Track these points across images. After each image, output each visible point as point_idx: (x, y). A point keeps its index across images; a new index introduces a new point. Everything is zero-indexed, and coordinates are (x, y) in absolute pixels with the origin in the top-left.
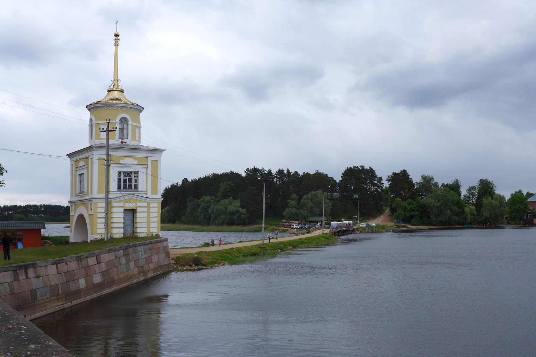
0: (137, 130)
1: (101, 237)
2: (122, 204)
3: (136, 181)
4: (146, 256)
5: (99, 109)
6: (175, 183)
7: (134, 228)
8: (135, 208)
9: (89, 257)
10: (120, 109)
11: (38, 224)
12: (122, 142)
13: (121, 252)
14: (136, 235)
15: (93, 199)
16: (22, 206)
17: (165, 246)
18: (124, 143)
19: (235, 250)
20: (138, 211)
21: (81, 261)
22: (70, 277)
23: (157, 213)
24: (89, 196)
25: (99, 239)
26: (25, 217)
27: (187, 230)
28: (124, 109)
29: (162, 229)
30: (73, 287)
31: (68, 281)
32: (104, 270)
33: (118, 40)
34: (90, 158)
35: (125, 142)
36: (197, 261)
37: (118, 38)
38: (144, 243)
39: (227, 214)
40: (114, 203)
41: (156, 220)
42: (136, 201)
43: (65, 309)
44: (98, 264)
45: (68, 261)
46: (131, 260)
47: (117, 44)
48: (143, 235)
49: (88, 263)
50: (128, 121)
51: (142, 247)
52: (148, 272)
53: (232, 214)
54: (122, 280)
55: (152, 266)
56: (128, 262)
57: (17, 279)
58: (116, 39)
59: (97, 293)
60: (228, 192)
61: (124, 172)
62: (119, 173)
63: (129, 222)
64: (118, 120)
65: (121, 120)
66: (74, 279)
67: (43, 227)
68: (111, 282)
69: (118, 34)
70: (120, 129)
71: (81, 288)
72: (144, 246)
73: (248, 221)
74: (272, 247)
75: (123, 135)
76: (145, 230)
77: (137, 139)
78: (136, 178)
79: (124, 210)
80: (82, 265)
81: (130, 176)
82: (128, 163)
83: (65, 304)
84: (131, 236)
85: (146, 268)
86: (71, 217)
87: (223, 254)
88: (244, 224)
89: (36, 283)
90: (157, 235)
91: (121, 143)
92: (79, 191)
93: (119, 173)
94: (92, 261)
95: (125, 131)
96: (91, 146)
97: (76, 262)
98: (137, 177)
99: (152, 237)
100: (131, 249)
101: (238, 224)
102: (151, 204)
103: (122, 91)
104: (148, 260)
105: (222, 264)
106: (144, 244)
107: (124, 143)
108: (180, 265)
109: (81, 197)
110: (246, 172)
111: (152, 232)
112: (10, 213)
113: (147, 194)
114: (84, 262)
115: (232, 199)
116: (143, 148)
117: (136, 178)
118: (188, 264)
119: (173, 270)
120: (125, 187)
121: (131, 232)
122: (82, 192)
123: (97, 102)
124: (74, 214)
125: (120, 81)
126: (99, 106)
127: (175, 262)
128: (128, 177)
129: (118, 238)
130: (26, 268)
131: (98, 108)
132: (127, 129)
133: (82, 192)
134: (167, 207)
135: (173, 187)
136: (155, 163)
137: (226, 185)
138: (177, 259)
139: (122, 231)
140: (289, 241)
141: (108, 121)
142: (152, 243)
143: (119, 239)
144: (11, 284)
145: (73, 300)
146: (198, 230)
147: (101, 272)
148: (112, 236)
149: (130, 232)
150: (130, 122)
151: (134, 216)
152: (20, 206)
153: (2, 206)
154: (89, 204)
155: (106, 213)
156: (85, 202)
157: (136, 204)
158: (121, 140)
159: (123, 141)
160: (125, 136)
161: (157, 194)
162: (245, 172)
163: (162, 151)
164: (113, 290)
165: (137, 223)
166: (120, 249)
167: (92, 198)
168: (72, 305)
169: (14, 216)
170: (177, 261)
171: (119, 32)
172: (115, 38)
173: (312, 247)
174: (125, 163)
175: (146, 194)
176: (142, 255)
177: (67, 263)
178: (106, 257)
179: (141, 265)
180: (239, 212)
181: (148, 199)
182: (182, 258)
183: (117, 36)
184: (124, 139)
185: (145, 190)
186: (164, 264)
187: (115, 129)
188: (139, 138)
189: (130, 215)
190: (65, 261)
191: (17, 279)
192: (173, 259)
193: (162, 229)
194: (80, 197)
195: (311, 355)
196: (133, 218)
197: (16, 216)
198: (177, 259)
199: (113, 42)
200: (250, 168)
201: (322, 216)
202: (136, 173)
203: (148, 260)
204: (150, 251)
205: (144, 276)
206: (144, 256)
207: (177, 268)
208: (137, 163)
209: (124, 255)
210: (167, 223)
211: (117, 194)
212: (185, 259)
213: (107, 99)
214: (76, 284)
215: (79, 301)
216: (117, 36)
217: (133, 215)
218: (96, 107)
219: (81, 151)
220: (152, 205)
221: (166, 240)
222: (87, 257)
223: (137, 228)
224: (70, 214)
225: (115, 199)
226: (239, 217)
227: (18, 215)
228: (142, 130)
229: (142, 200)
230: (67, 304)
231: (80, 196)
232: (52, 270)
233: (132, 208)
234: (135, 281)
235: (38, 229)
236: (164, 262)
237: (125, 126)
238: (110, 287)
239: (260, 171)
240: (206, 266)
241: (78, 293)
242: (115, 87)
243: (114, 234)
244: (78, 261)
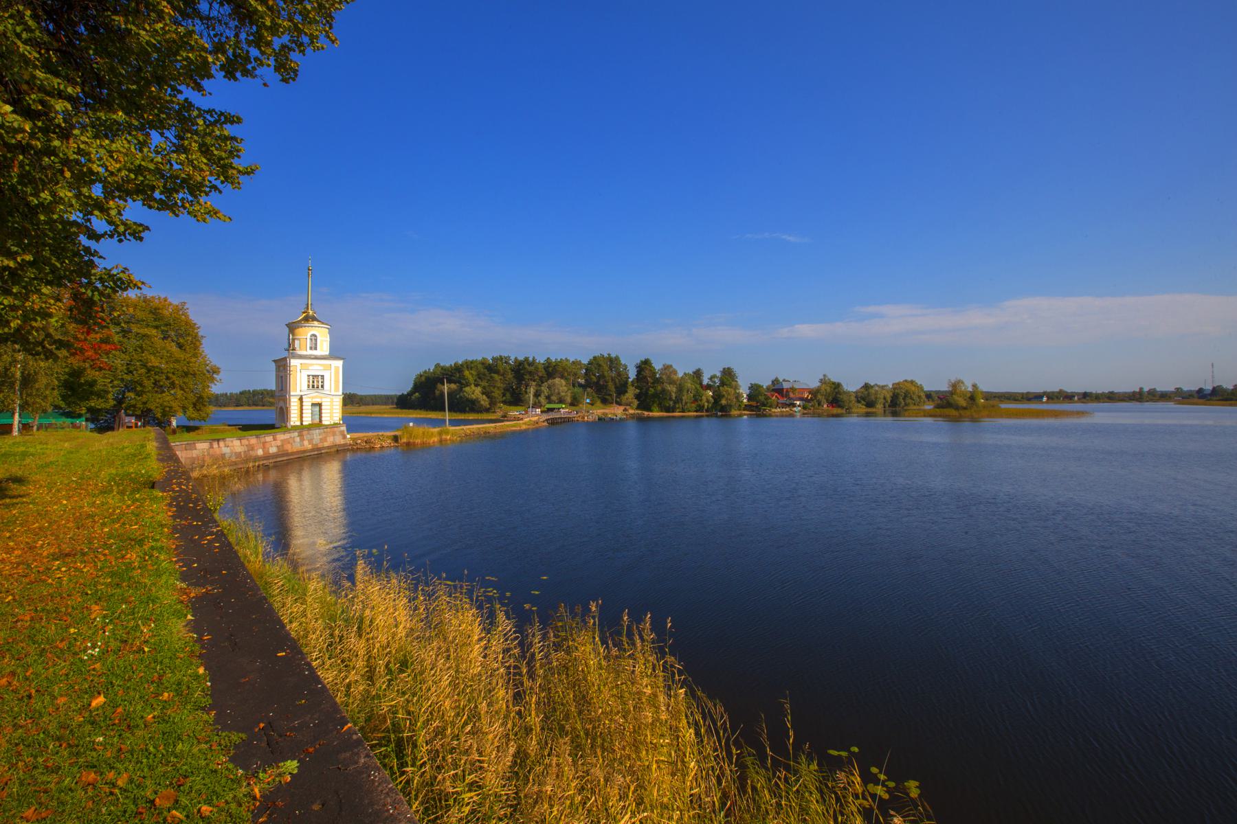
13: (296, 434)
22: (252, 448)
57: (211, 447)
64: (309, 337)
89: (226, 450)
114: (263, 440)
120: (313, 386)
130: (218, 440)
139: (310, 419)
140: (1126, 393)
144: (208, 450)
173: (1102, 416)
191: (211, 447)
201: (445, 411)
202: (323, 376)
232: (237, 443)
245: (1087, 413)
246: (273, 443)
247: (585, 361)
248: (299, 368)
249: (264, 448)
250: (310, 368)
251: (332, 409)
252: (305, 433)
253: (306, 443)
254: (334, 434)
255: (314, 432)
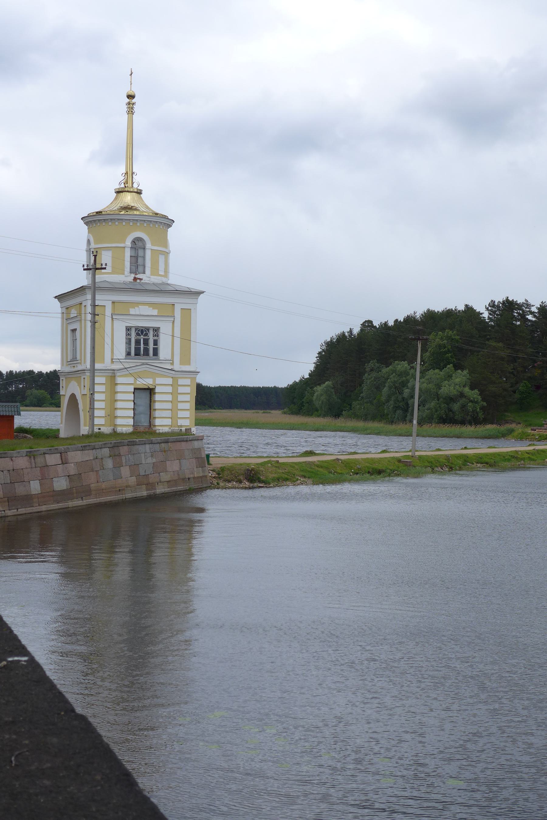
0: (162, 259)
1: (99, 431)
2: (131, 380)
3: (156, 343)
4: (154, 460)
5: (105, 223)
6: (346, 330)
7: (151, 418)
8: (151, 387)
9: (48, 454)
10: (131, 224)
11: (10, 408)
12: (135, 279)
13: (106, 451)
14: (154, 429)
15: (86, 371)
16: (44, 372)
17: (196, 447)
18: (138, 281)
19: (341, 462)
20: (157, 390)
21: (34, 458)
23: (189, 396)
26: (49, 396)
27: (354, 430)
28: (138, 224)
29: (199, 423)
30: (20, 490)
31: (13, 482)
32: (72, 472)
33: (133, 104)
34: (83, 304)
35: (141, 279)
36: (252, 475)
37: (134, 101)
38: (152, 440)
39: (441, 400)
40: (118, 378)
41: (187, 406)
42: (153, 376)
43: (8, 516)
44: (63, 463)
45: (15, 456)
46: (124, 464)
47: (131, 110)
48: (166, 429)
49: (46, 461)
50: (146, 243)
51: (147, 446)
52: (157, 485)
53: (450, 400)
54: (104, 491)
55: (165, 477)
56: (118, 466)
58: (129, 103)
59: (58, 503)
60: (446, 353)
61: (137, 329)
62: (128, 329)
63: (143, 408)
64: (128, 243)
65: (133, 242)
66: (22, 480)
67: (16, 413)
68: (87, 492)
69: (133, 94)
70: (132, 258)
71: (33, 493)
72: (150, 445)
73: (483, 416)
74: (429, 462)
75: (137, 267)
76: (168, 422)
77: (162, 273)
78: (156, 338)
79: (135, 389)
80: (35, 464)
81: (146, 335)
82: (142, 313)
83: (8, 511)
84: (147, 430)
85: (153, 479)
86: (62, 398)
87: (310, 468)
88: (475, 421)
90: (188, 431)
91: (133, 280)
92: (72, 357)
93: (128, 330)
94: (53, 459)
95: (140, 260)
96: (82, 287)
97: (26, 459)
98: (158, 337)
99: (180, 433)
100: (126, 448)
101: (463, 423)
102: (179, 380)
103: (139, 192)
104: (160, 467)
105: (299, 482)
106: (152, 443)
107: (138, 281)
108: (224, 480)
109: (73, 366)
110: (490, 308)
111: (181, 426)
112: (21, 386)
113: (173, 365)
114: (40, 460)
115: (453, 368)
116: (171, 288)
117: (156, 338)
118: (236, 480)
119: (210, 488)
120: (137, 354)
121: (146, 424)
122: (74, 359)
123: (97, 213)
124: (66, 392)
126: (99, 220)
127: (217, 476)
128: (142, 336)
129: (125, 432)
131: (104, 221)
132: (144, 257)
133: (74, 359)
134: (327, 383)
135: (342, 338)
136: (187, 313)
137: (442, 339)
138: (220, 470)
139: (131, 422)
141: (95, 254)
142: (168, 442)
143: (126, 434)
145: (19, 507)
146: (368, 431)
147: (68, 476)
148: (115, 430)
149: (146, 424)
150: (149, 245)
151: (152, 399)
152: (40, 374)
153: (4, 372)
154: (82, 377)
155: (92, 394)
156: (76, 376)
157: (154, 381)
158: (133, 276)
159: (137, 276)
160: (140, 269)
161: (190, 365)
162: (487, 309)
163: (199, 293)
164: (87, 503)
165: (155, 410)
166: (103, 446)
167: (85, 369)
168: (18, 513)
169: (29, 392)
170: (220, 474)
171: (135, 90)
172: (128, 100)
174: (138, 313)
175: (172, 364)
176: (146, 458)
177: (13, 458)
178: (76, 456)
179: (142, 473)
181: (173, 372)
182: (228, 469)
183: (131, 97)
184: (139, 273)
185: (170, 358)
186: (192, 476)
187: (104, 266)
189: (144, 398)
190: (10, 456)
192: (213, 471)
193: (199, 423)
196: (151, 402)
197: (31, 394)
198: (220, 470)
199: (125, 108)
200: (499, 298)
202: (156, 330)
203: (160, 467)
204: (164, 454)
205: (147, 490)
206: (150, 460)
207: (218, 484)
208: (156, 314)
209: (110, 456)
210: (324, 416)
211: (130, 364)
212: (233, 471)
213: (116, 207)
214: (25, 486)
215: (29, 510)
216: (131, 97)
217: (151, 398)
218: (95, 221)
219: (70, 294)
220: (181, 382)
221: (200, 439)
222: (44, 454)
223: (155, 418)
225: (119, 371)
226: (463, 406)
227: (36, 391)
229: (156, 372)
230: (11, 511)
233: (147, 387)
234: (129, 495)
235: (9, 416)
236: (193, 473)
237: (141, 253)
238: (82, 498)
239: (519, 306)
240: (266, 484)
241: (28, 499)
242: (127, 186)
243: (118, 426)
244: (30, 457)
245: (527, 453)
246: (60, 468)
247: (501, 301)
248: (108, 311)
249: (43, 479)
250: (132, 311)
251: (174, 402)
252: (124, 450)
253: (125, 471)
254: (180, 457)
255: (141, 448)
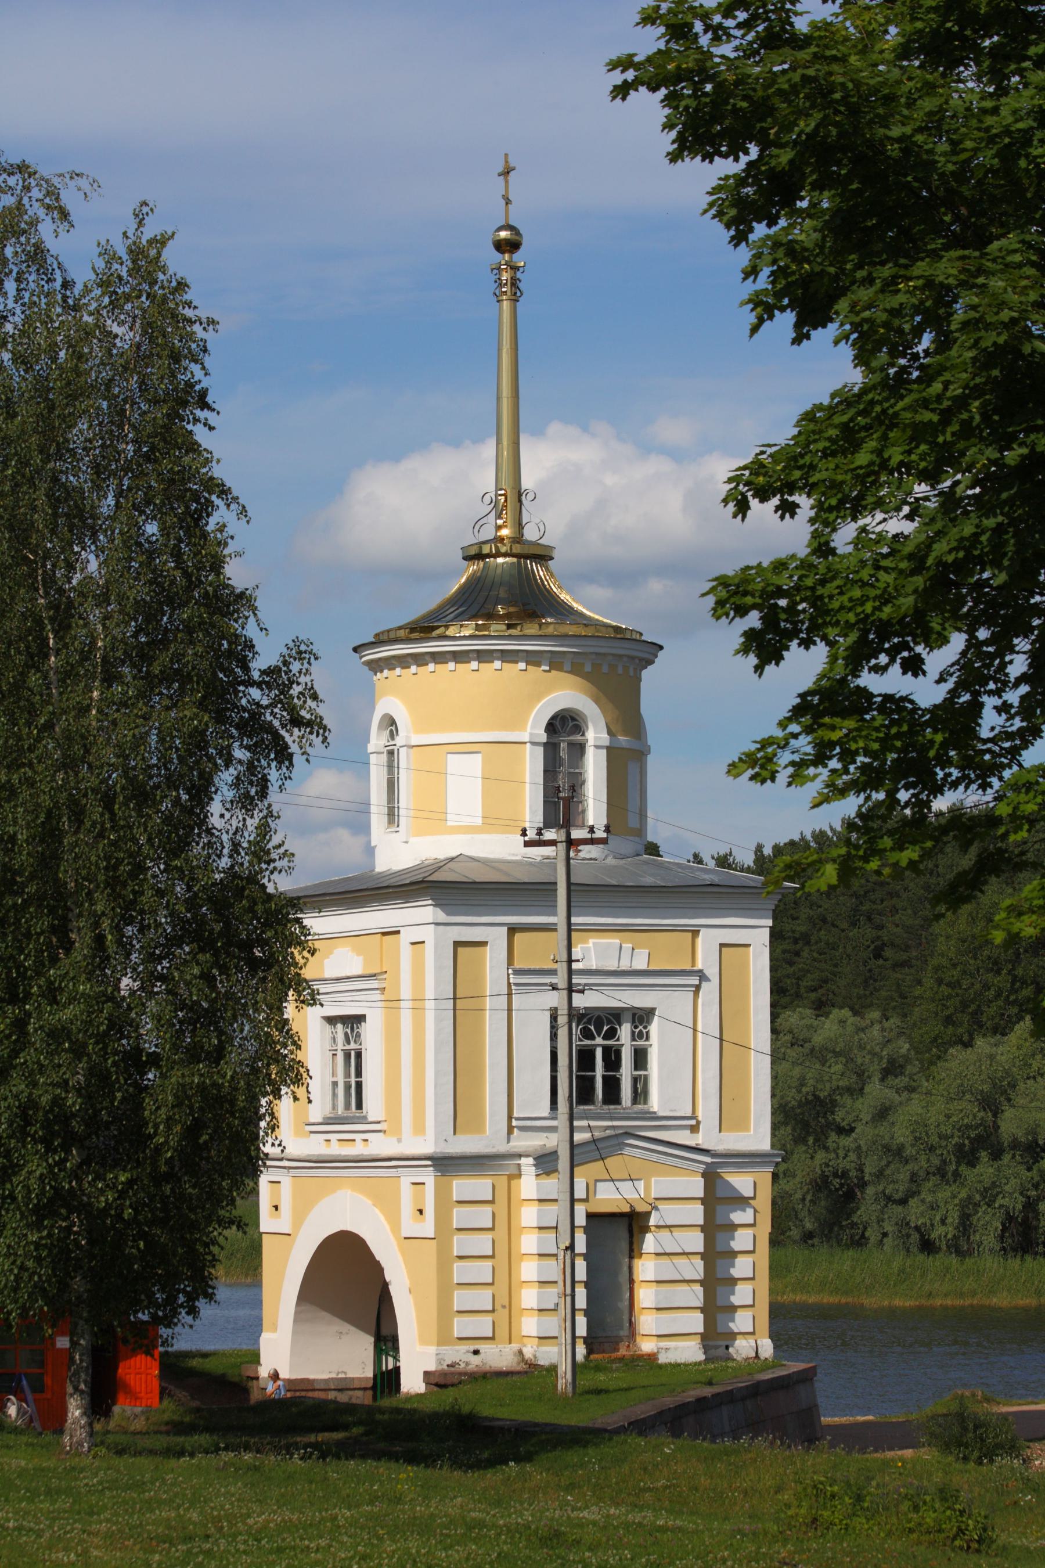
0: (633, 768)
8: (641, 1208)
24: (399, 1140)
25: (463, 1365)
81: (612, 1034)
98: (647, 1039)
125: (531, 496)
180: (995, 1115)
188: (643, 815)
194: (334, 1142)
195: (826, 58)
224: (262, 1229)
228: (653, 762)
231: (333, 1137)
233: (626, 1209)
